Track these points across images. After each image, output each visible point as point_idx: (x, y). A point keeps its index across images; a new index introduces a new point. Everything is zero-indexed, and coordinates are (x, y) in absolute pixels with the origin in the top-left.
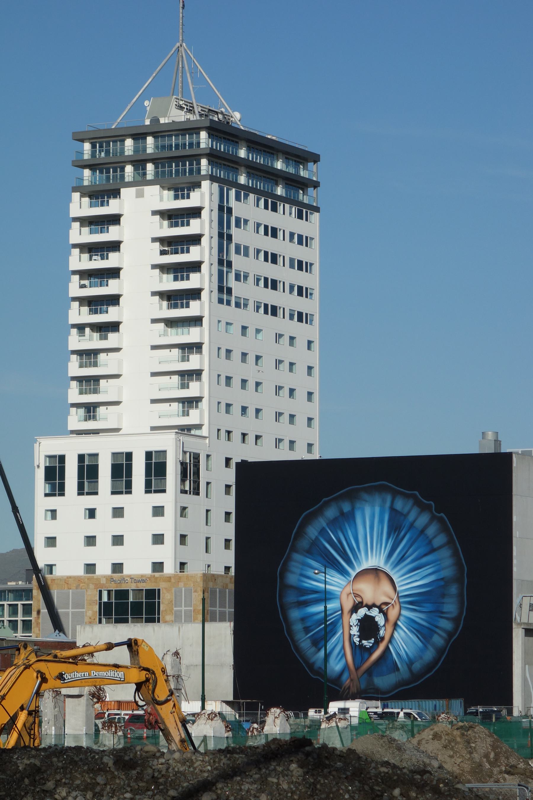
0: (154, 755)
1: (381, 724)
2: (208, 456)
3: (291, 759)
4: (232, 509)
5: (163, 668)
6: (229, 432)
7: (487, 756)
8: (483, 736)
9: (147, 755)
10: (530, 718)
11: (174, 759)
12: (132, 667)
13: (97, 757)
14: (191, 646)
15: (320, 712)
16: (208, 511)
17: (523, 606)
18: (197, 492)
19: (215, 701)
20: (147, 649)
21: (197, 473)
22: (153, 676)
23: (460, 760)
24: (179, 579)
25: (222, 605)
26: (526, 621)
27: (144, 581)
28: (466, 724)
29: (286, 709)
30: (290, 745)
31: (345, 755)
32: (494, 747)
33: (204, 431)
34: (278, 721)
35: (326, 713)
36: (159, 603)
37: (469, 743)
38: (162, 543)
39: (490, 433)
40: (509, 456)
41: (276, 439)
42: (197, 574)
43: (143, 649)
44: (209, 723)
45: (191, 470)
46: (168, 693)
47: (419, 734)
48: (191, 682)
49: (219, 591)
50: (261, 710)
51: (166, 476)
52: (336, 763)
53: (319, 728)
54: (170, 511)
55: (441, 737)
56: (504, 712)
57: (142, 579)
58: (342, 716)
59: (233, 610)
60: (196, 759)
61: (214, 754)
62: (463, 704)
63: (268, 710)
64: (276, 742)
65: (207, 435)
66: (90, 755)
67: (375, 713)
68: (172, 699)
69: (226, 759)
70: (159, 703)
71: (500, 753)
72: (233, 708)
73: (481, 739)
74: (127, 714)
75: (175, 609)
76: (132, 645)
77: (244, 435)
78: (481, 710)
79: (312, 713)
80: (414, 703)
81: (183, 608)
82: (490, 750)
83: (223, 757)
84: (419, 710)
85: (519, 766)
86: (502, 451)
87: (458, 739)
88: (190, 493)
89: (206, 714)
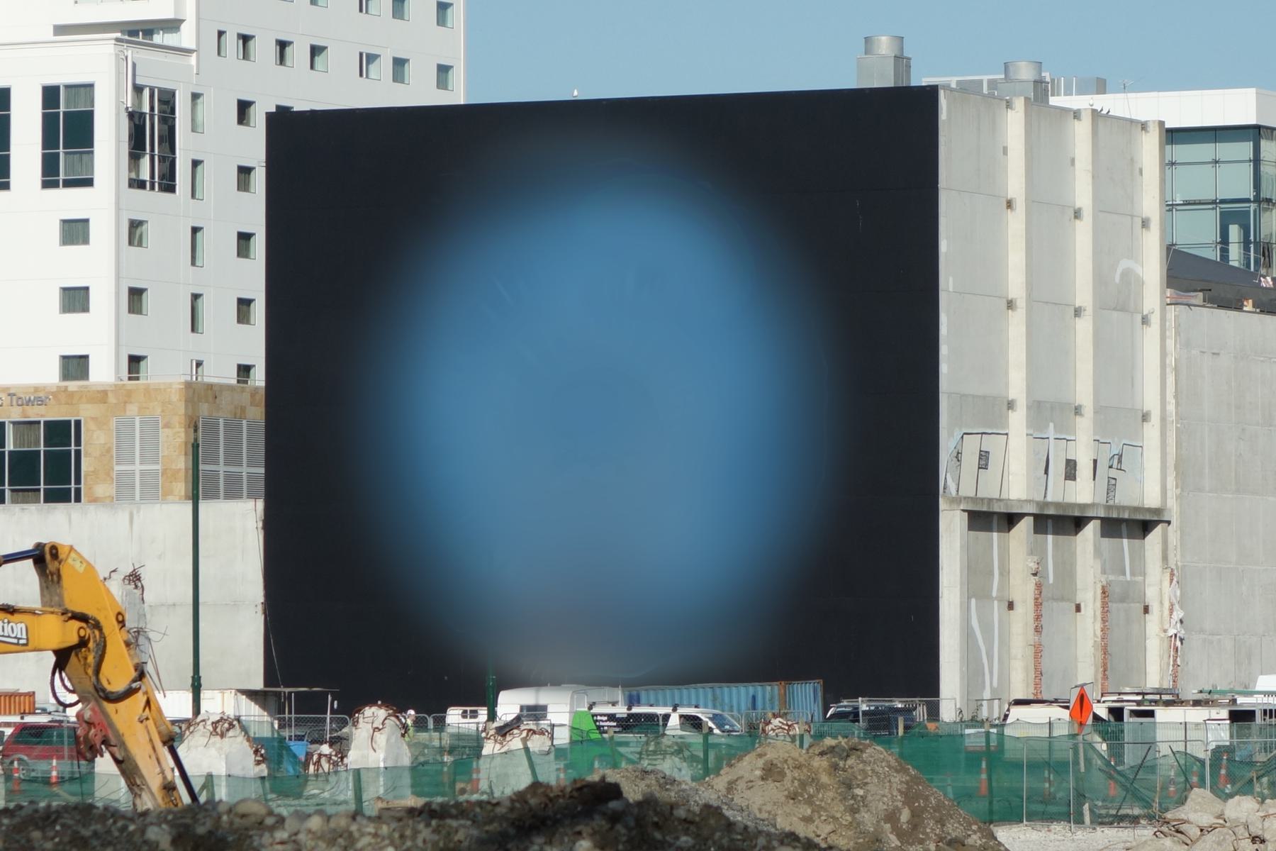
0: (261, 823)
1: (626, 744)
2: (195, 97)
3: (578, 828)
4: (258, 227)
5: (119, 613)
6: (245, 39)
7: (892, 817)
8: (882, 769)
9: (245, 822)
10: (987, 725)
11: (309, 831)
12: (45, 612)
13: (132, 828)
14: (160, 557)
15: (474, 714)
16: (195, 230)
17: (964, 458)
18: (168, 184)
19: (222, 690)
20: (80, 568)
21: (169, 138)
22: (97, 632)
23: (829, 828)
24: (128, 396)
25: (233, 459)
26: (973, 495)
27: (41, 402)
28: (843, 742)
29: (397, 705)
30: (571, 797)
31: (697, 819)
32: (909, 797)
33: (186, 37)
34: (381, 738)
35: (492, 716)
36: (78, 453)
37: (849, 787)
38: (85, 309)
39: (884, 38)
40: (929, 95)
41: (361, 54)
42: (171, 384)
43: (73, 567)
44: (214, 743)
45: (153, 129)
46: (134, 674)
47: (731, 766)
48: (168, 649)
49: (225, 425)
50: (333, 712)
51: (92, 145)
52: (677, 838)
53: (479, 756)
54: (105, 231)
55: (782, 774)
56: (921, 713)
57: (38, 397)
58: (531, 725)
59: (262, 470)
60: (359, 830)
61: (400, 820)
62: (820, 694)
63: (358, 712)
64: (541, 790)
65: (193, 46)
66: (115, 822)
67: (611, 717)
68: (143, 688)
69: (430, 830)
70: (112, 697)
71: (924, 810)
72: (264, 706)
73: (879, 778)
74: (8, 725)
75: (117, 468)
76: (44, 559)
77: (283, 45)
78: (864, 707)
79: (454, 716)
80: (703, 691)
81: (138, 467)
82: (900, 804)
83: (421, 826)
84: (715, 707)
85: (970, 841)
86: (913, 84)
87: (824, 779)
88: (152, 188)
89: (209, 723)
